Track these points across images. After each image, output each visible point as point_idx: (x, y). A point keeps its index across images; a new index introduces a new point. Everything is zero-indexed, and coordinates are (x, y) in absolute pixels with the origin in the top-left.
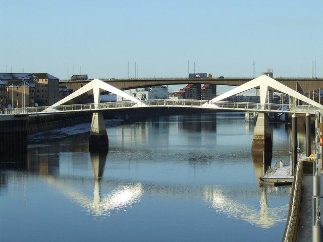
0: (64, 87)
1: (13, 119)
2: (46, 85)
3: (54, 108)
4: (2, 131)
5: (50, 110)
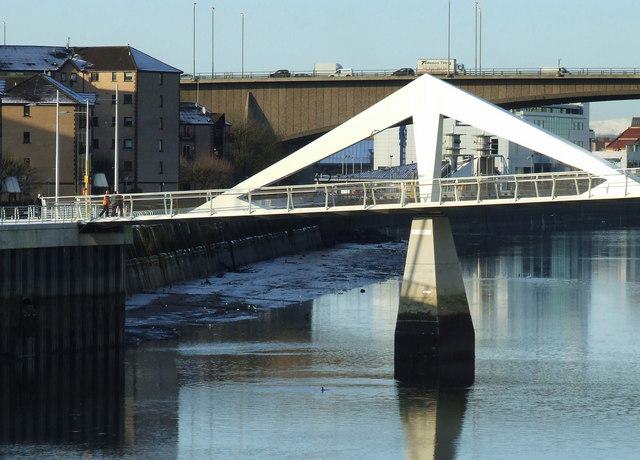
0: (190, 107)
1: (72, 240)
2: (127, 98)
3: (244, 197)
4: (6, 294)
5: (226, 204)
